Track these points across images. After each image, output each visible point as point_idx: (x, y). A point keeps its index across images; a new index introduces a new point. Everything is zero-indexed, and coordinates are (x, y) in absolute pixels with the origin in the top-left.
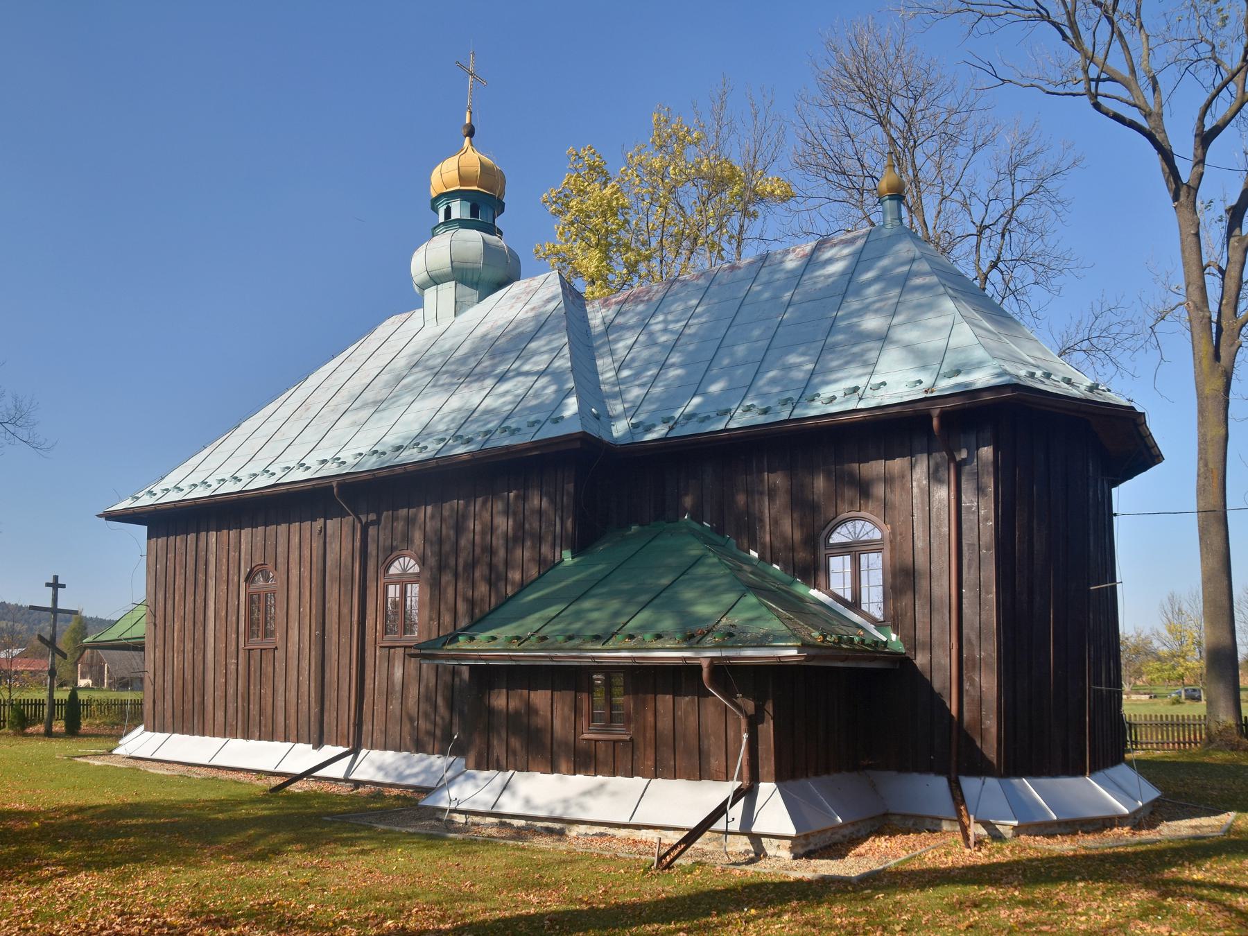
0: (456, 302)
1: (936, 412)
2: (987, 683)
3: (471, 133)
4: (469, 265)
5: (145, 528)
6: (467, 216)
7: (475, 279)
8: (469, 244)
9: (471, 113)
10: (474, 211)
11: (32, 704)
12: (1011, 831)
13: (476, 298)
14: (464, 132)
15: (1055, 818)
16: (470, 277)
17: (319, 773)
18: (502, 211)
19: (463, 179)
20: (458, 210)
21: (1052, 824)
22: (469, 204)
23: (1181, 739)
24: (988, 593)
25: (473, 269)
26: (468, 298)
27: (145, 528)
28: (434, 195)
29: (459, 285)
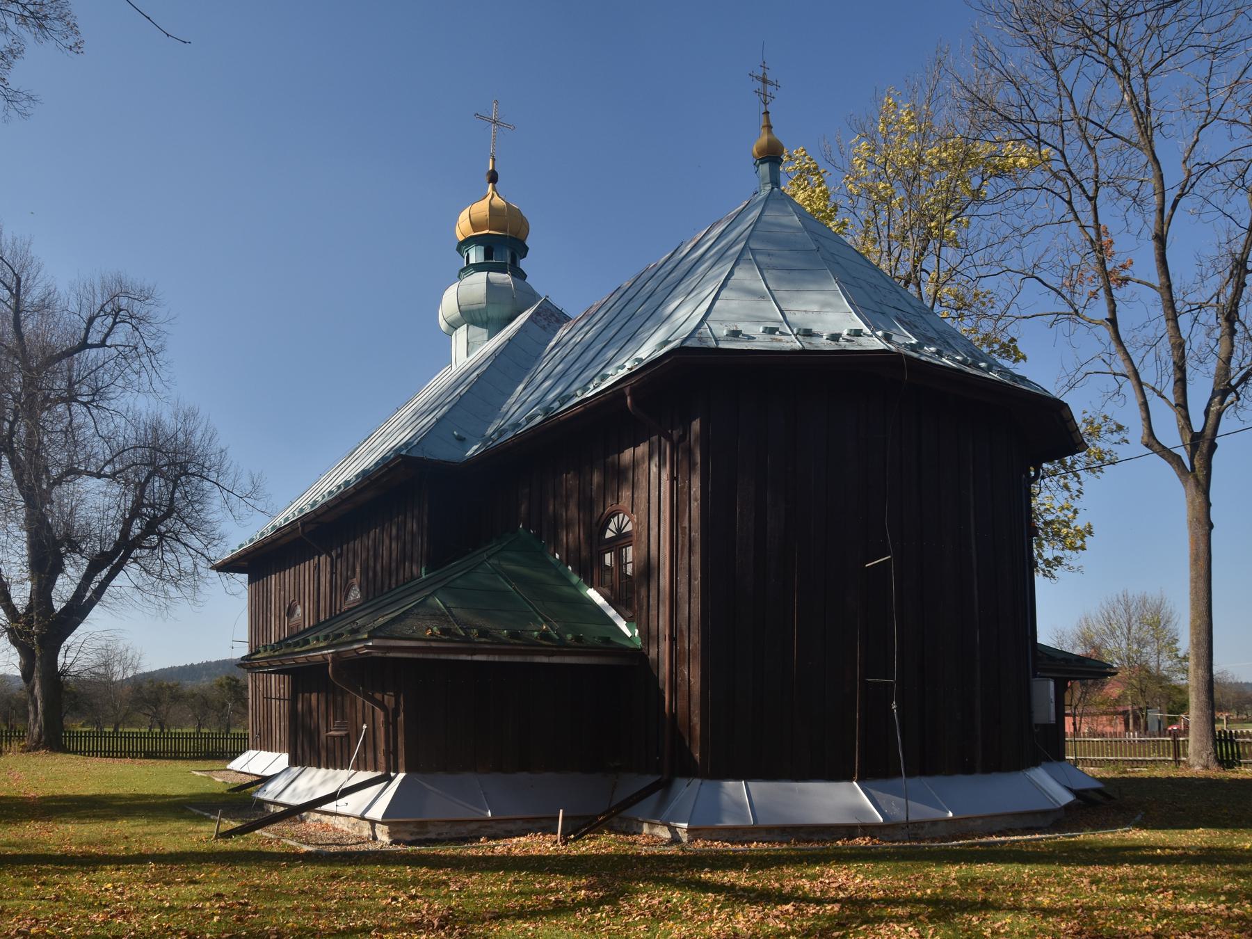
0: (468, 343)
1: (627, 391)
2: (693, 675)
3: (493, 177)
4: (475, 307)
5: (246, 576)
6: (481, 259)
7: (485, 318)
8: (474, 286)
9: (494, 160)
10: (488, 255)
11: (89, 752)
12: (686, 835)
13: (486, 337)
14: (486, 179)
15: (881, 819)
16: (478, 317)
17: (326, 807)
18: (525, 256)
19: (475, 225)
20: (475, 255)
21: (878, 827)
22: (483, 248)
23: (269, 696)
24: (696, 580)
25: (479, 310)
26: (479, 338)
27: (246, 576)
28: (461, 238)
29: (471, 327)
